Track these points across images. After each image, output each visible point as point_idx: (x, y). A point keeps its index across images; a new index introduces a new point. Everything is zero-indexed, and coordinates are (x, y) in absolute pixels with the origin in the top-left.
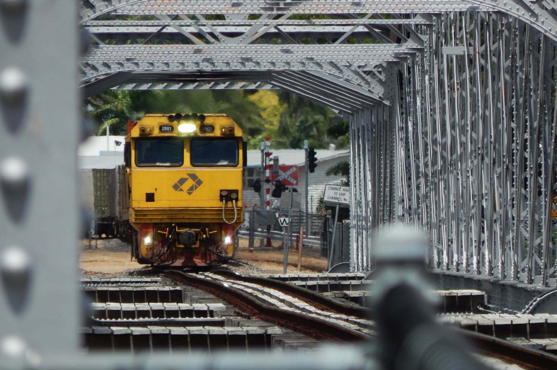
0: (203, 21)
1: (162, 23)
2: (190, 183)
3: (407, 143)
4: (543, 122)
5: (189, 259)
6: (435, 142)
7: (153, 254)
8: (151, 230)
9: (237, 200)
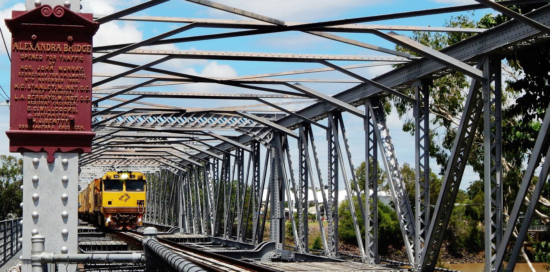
2: (125, 197)
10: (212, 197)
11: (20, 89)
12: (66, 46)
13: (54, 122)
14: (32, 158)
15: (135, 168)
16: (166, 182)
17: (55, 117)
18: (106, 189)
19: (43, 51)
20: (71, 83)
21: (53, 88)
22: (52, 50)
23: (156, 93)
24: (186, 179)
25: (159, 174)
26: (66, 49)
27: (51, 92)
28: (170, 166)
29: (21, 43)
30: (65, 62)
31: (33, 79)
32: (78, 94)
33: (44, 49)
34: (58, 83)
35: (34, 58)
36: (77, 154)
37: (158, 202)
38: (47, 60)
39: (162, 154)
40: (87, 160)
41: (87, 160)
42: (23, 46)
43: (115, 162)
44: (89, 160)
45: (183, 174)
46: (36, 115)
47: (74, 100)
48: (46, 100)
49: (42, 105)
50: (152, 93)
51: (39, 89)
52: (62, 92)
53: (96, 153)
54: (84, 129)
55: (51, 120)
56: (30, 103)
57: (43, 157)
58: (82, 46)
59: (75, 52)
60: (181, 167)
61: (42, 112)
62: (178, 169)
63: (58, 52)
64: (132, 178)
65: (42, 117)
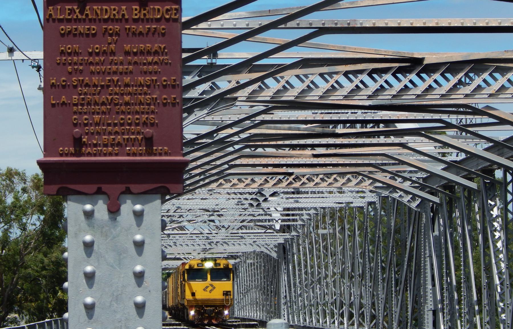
0: (186, 254)
1: (176, 255)
2: (210, 288)
3: (238, 285)
4: (393, 256)
5: (210, 321)
6: (245, 285)
7: (195, 319)
8: (194, 308)
9: (230, 295)
10: (503, 265)
11: (60, 86)
12: (136, 10)
13: (119, 142)
14: (82, 204)
15: (318, 195)
16: (393, 228)
17: (120, 133)
19: (97, 20)
20: (145, 73)
21: (115, 83)
22: (112, 17)
23: (349, 24)
24: (441, 221)
25: (375, 209)
26: (136, 15)
27: (112, 90)
28: (401, 190)
29: (59, 7)
30: (136, 36)
31: (81, 68)
32: (158, 92)
33: (98, 16)
34: (124, 73)
35: (82, 31)
36: (159, 196)
37: (374, 279)
38: (104, 34)
39: (379, 161)
40: (197, 178)
41: (197, 178)
42: (62, 11)
43: (266, 181)
44: (203, 180)
45: (432, 208)
46: (87, 129)
47: (152, 103)
48: (103, 104)
49: (98, 113)
50: (341, 24)
51: (91, 86)
52: (130, 89)
53: (218, 162)
54: (170, 153)
55: (113, 139)
56: (77, 110)
57: (101, 203)
58: (163, 8)
59: (152, 19)
60: (428, 192)
61: (98, 124)
62: (419, 197)
63: (123, 20)
65: (98, 133)
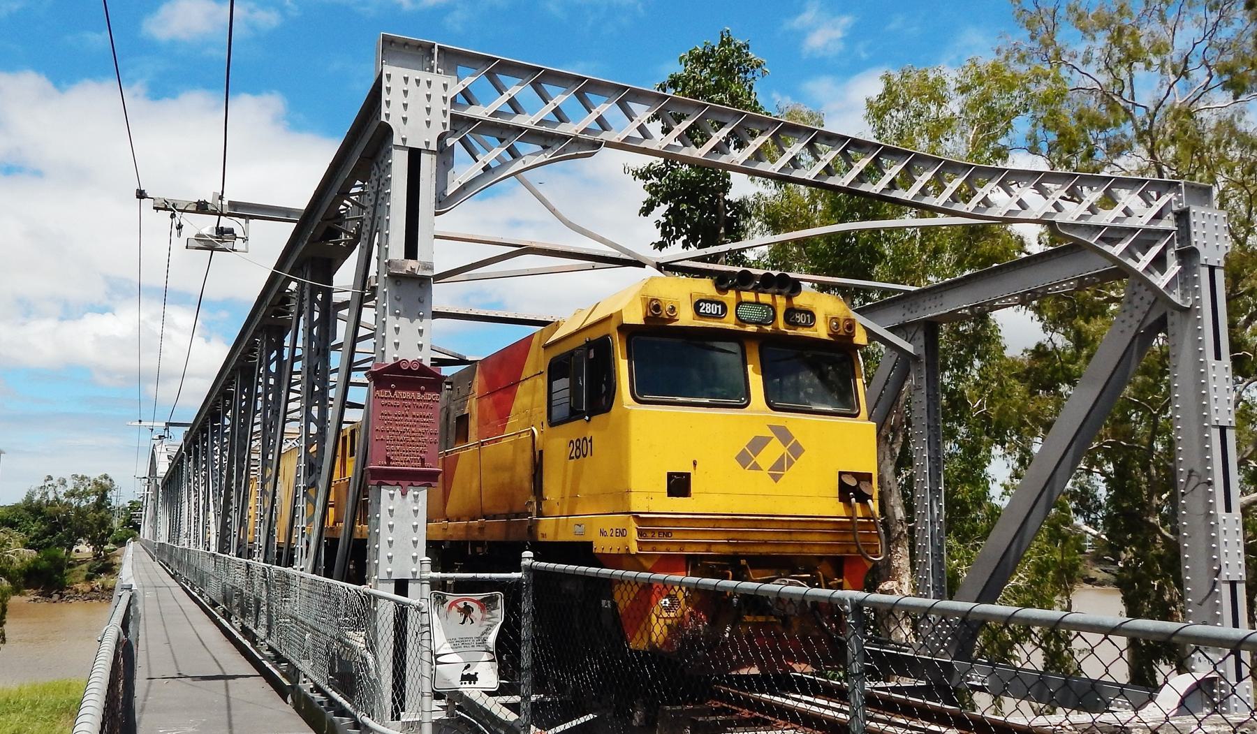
2: (775, 450)
18: (645, 390)
42: (383, 393)
64: (795, 325)
